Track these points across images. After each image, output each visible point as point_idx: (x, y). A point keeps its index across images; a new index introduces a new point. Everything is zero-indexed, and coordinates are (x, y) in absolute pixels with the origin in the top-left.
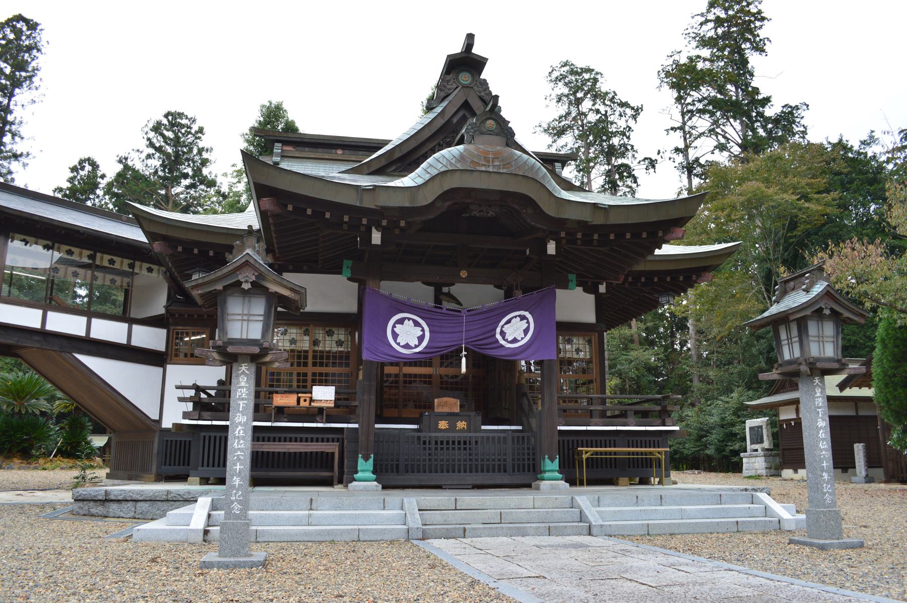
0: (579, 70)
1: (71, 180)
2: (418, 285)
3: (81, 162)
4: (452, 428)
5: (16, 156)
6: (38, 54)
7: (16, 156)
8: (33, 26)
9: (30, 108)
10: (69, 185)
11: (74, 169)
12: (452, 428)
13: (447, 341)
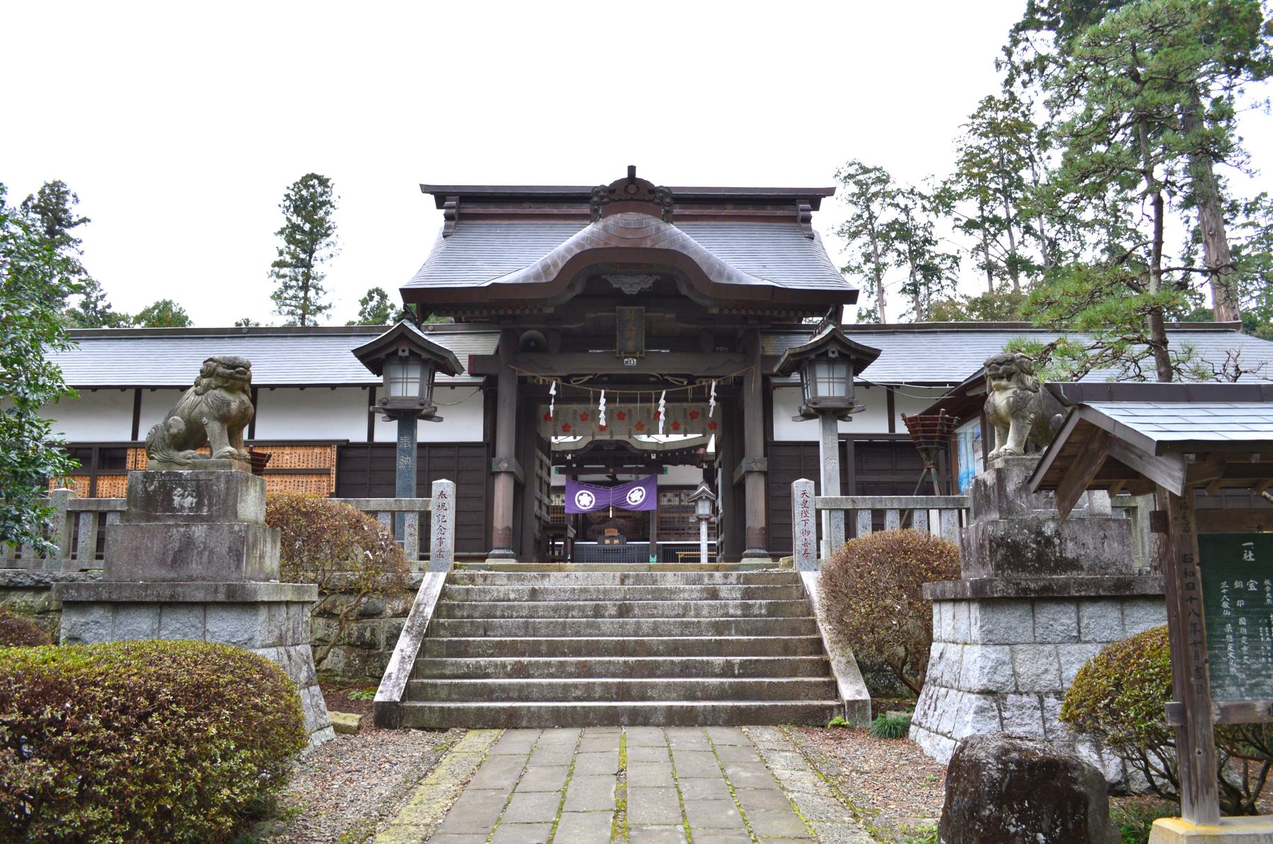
0: (1097, 227)
1: (361, 313)
2: (444, 481)
3: (370, 293)
4: (612, 543)
5: (319, 309)
6: (331, 210)
7: (319, 309)
8: (323, 182)
9: (328, 262)
10: (361, 318)
11: (364, 302)
12: (612, 543)
13: (603, 503)
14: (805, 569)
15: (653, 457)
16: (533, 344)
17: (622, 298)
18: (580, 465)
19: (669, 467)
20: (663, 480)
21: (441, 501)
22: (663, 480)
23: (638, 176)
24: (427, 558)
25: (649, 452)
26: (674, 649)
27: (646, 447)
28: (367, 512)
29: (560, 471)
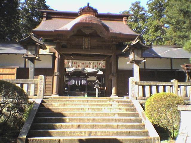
14: (19, 87)
15: (87, 75)
16: (64, 46)
17: (85, 36)
18: (71, 76)
19: (90, 77)
20: (88, 79)
21: (41, 81)
22: (88, 79)
23: (90, 6)
24: (36, 95)
25: (86, 74)
26: (104, 120)
27: (85, 72)
28: (144, 109)
29: (67, 77)
